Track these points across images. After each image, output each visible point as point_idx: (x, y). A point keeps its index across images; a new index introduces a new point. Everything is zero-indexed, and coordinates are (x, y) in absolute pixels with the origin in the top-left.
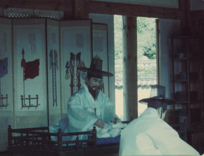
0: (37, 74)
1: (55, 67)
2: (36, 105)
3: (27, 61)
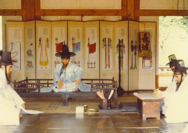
0: (95, 51)
1: (109, 47)
2: (94, 67)
3: (90, 44)
